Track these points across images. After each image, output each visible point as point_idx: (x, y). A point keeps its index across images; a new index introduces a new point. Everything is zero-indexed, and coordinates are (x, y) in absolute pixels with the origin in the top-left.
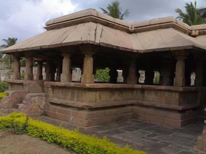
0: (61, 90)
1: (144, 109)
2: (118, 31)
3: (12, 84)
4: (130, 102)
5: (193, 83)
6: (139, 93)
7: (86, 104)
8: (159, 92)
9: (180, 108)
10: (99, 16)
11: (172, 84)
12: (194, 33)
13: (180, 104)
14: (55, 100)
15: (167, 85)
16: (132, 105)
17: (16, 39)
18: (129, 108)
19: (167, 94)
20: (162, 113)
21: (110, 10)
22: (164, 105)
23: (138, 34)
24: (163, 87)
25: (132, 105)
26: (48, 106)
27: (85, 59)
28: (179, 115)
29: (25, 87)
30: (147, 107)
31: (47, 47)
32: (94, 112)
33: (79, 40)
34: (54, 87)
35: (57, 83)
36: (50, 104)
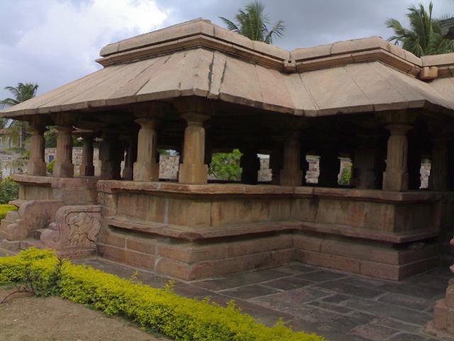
0: (133, 200)
1: (317, 241)
4: (286, 225)
6: (306, 205)
7: (191, 230)
8: (351, 204)
9: (397, 238)
10: (216, 36)
11: (378, 185)
12: (427, 73)
13: (396, 230)
14: (122, 221)
15: (368, 188)
16: (291, 231)
17: (36, 87)
19: (368, 207)
20: (357, 249)
21: (242, 22)
24: (358, 193)
25: (291, 231)
28: (394, 255)
30: (324, 235)
31: (104, 104)
34: (118, 193)
35: (126, 184)
36: (109, 230)
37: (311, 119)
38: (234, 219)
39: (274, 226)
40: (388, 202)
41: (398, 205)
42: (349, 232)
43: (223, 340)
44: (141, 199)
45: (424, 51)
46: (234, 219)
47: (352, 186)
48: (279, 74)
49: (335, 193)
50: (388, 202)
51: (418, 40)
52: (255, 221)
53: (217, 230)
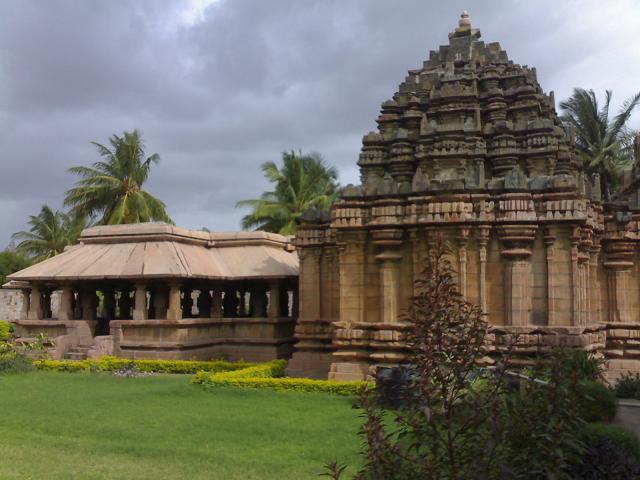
2: (195, 247)
4: (218, 340)
5: (631, 263)
6: (228, 328)
9: (276, 341)
13: (275, 337)
14: (129, 343)
16: (220, 344)
18: (218, 347)
19: (261, 327)
20: (257, 348)
22: (259, 340)
23: (220, 249)
25: (220, 344)
26: (118, 351)
27: (171, 292)
28: (274, 349)
29: (68, 330)
30: (238, 344)
32: (187, 351)
33: (169, 272)
34: (125, 327)
36: (120, 349)
40: (270, 324)
41: (275, 325)
42: (252, 340)
45: (297, 165)
46: (203, 337)
47: (250, 315)
48: (205, 250)
49: (491, 292)
50: (270, 324)
51: (289, 181)
52: (203, 338)
53: (209, 341)
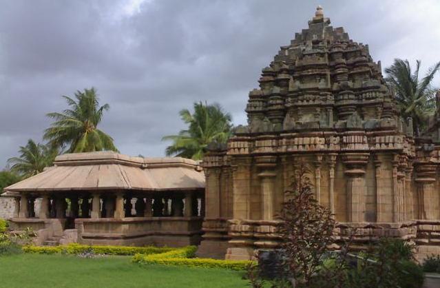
0: (94, 226)
1: (161, 237)
3: (20, 224)
4: (149, 232)
7: (122, 234)
9: (189, 233)
13: (189, 230)
14: (88, 234)
16: (151, 235)
17: (196, 104)
18: (149, 237)
19: (179, 223)
20: (176, 238)
22: (177, 232)
23: (151, 170)
25: (151, 235)
29: (46, 225)
34: (85, 224)
37: (157, 192)
38: (136, 230)
39: (144, 233)
41: (189, 221)
42: (173, 232)
43: (390, 286)
44: (97, 226)
48: (141, 170)
52: (139, 231)
